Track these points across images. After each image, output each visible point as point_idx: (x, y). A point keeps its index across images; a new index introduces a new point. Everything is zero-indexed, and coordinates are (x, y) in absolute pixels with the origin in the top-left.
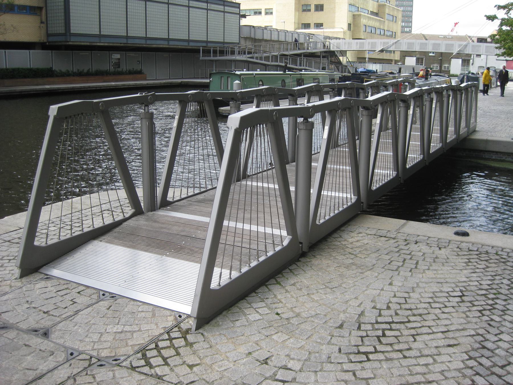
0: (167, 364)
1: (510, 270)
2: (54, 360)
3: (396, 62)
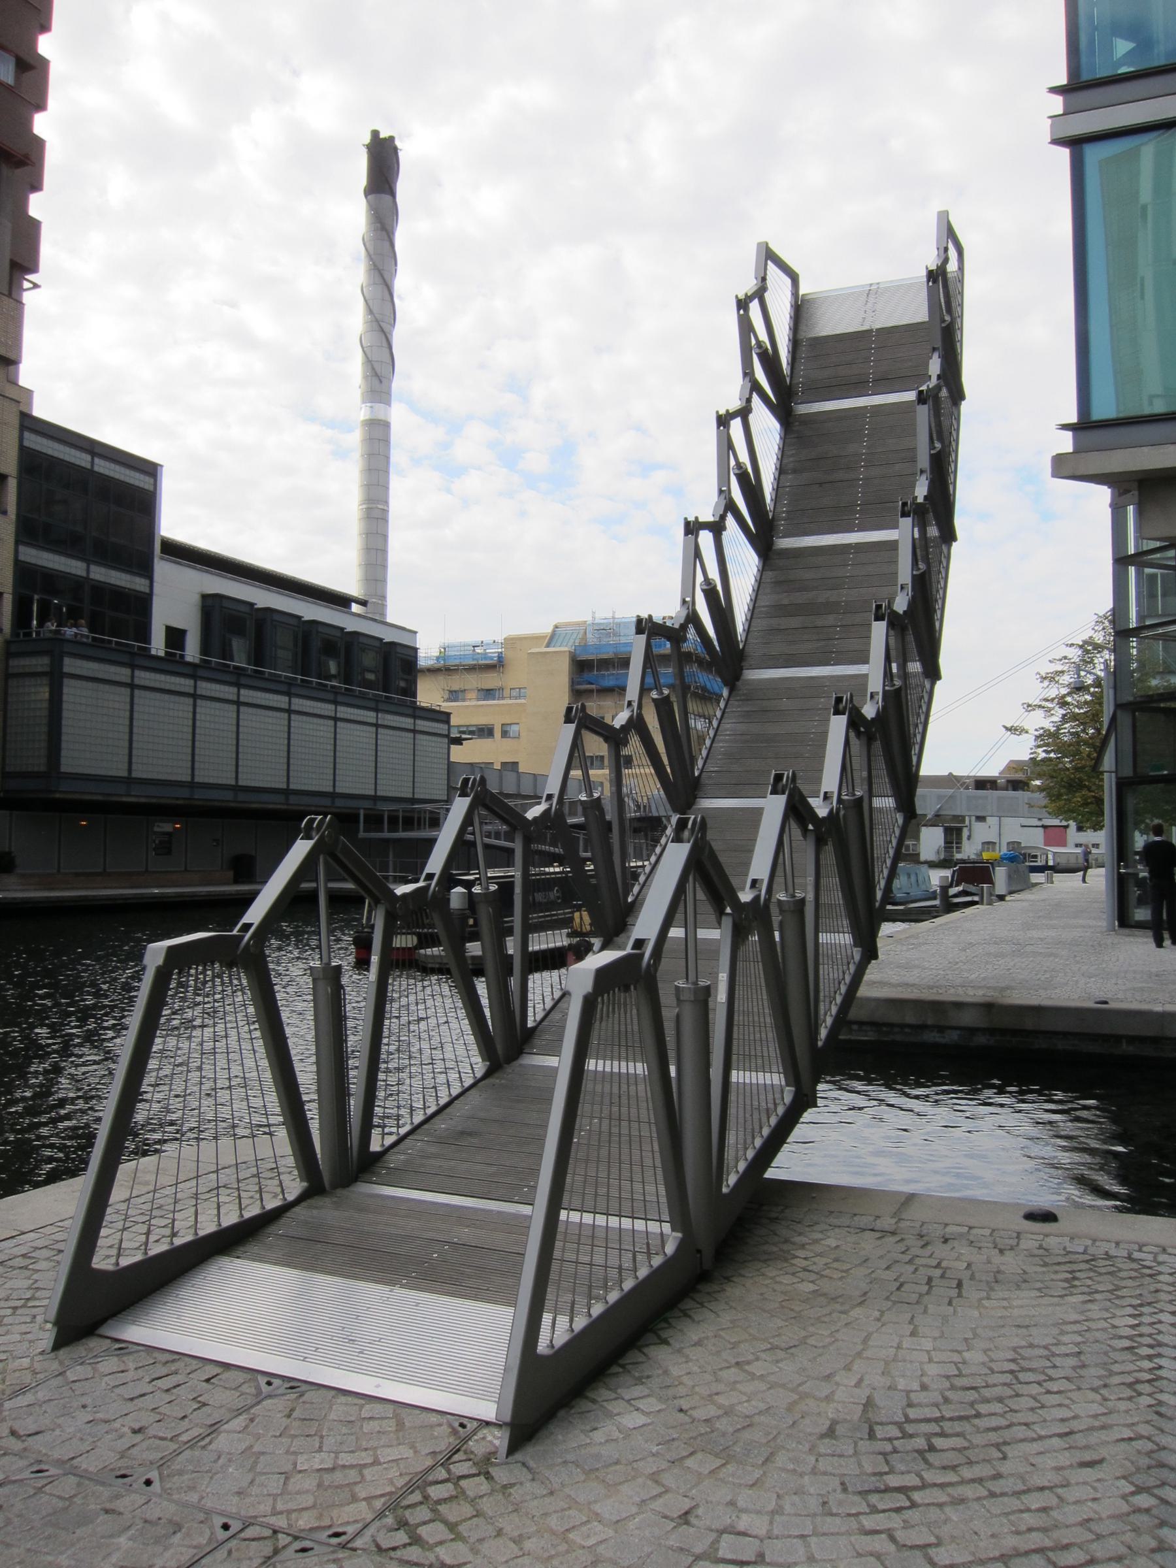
0: (459, 1537)
1: (1170, 1293)
2: (186, 1543)
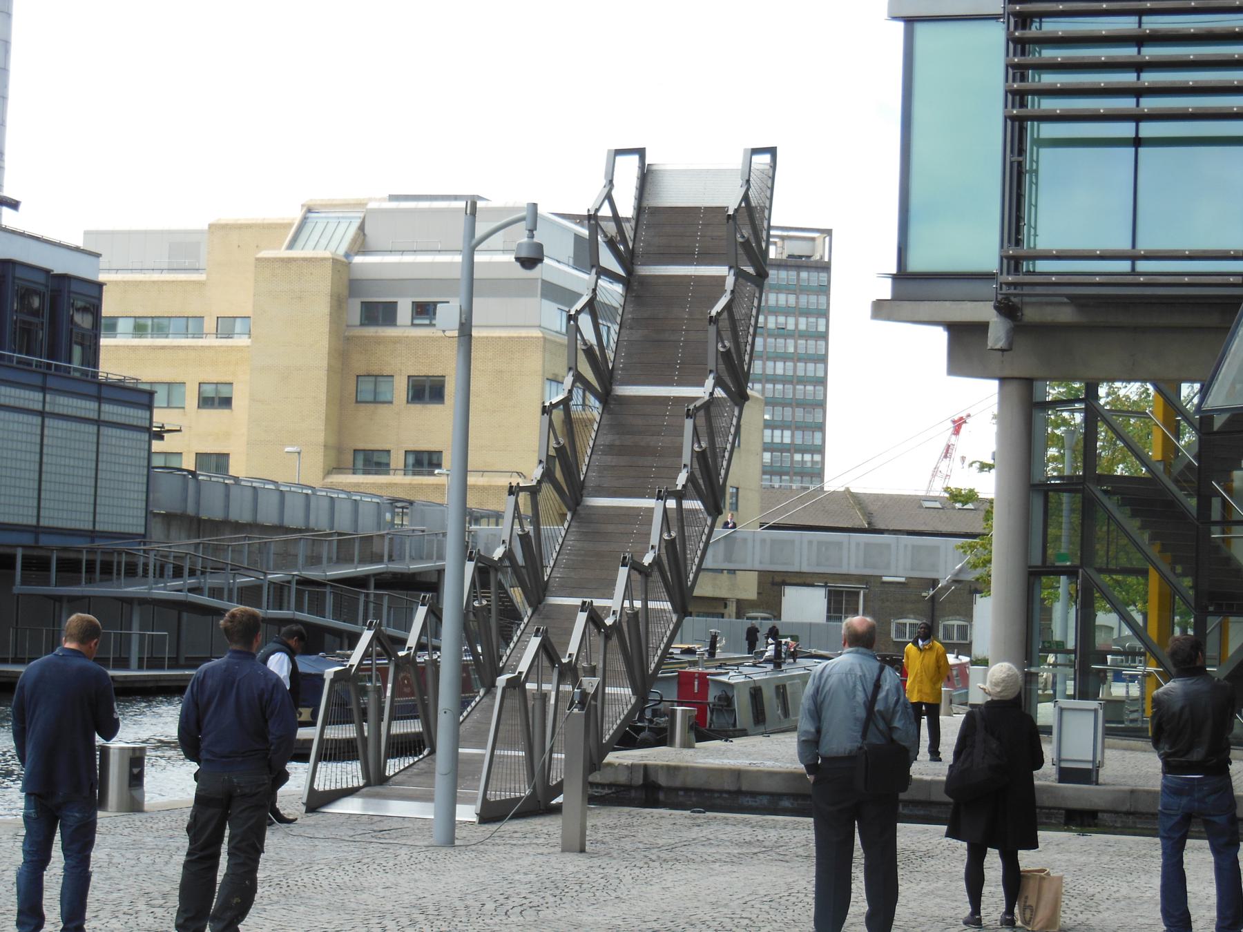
3: (742, 607)
